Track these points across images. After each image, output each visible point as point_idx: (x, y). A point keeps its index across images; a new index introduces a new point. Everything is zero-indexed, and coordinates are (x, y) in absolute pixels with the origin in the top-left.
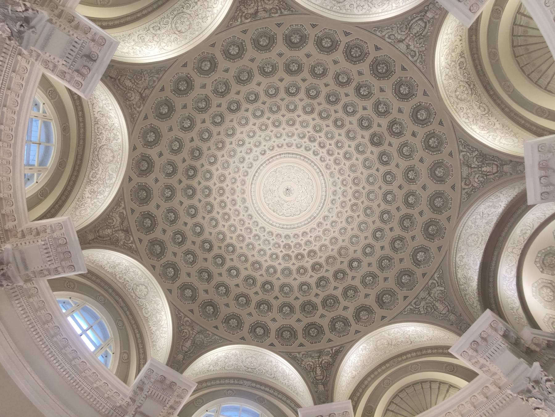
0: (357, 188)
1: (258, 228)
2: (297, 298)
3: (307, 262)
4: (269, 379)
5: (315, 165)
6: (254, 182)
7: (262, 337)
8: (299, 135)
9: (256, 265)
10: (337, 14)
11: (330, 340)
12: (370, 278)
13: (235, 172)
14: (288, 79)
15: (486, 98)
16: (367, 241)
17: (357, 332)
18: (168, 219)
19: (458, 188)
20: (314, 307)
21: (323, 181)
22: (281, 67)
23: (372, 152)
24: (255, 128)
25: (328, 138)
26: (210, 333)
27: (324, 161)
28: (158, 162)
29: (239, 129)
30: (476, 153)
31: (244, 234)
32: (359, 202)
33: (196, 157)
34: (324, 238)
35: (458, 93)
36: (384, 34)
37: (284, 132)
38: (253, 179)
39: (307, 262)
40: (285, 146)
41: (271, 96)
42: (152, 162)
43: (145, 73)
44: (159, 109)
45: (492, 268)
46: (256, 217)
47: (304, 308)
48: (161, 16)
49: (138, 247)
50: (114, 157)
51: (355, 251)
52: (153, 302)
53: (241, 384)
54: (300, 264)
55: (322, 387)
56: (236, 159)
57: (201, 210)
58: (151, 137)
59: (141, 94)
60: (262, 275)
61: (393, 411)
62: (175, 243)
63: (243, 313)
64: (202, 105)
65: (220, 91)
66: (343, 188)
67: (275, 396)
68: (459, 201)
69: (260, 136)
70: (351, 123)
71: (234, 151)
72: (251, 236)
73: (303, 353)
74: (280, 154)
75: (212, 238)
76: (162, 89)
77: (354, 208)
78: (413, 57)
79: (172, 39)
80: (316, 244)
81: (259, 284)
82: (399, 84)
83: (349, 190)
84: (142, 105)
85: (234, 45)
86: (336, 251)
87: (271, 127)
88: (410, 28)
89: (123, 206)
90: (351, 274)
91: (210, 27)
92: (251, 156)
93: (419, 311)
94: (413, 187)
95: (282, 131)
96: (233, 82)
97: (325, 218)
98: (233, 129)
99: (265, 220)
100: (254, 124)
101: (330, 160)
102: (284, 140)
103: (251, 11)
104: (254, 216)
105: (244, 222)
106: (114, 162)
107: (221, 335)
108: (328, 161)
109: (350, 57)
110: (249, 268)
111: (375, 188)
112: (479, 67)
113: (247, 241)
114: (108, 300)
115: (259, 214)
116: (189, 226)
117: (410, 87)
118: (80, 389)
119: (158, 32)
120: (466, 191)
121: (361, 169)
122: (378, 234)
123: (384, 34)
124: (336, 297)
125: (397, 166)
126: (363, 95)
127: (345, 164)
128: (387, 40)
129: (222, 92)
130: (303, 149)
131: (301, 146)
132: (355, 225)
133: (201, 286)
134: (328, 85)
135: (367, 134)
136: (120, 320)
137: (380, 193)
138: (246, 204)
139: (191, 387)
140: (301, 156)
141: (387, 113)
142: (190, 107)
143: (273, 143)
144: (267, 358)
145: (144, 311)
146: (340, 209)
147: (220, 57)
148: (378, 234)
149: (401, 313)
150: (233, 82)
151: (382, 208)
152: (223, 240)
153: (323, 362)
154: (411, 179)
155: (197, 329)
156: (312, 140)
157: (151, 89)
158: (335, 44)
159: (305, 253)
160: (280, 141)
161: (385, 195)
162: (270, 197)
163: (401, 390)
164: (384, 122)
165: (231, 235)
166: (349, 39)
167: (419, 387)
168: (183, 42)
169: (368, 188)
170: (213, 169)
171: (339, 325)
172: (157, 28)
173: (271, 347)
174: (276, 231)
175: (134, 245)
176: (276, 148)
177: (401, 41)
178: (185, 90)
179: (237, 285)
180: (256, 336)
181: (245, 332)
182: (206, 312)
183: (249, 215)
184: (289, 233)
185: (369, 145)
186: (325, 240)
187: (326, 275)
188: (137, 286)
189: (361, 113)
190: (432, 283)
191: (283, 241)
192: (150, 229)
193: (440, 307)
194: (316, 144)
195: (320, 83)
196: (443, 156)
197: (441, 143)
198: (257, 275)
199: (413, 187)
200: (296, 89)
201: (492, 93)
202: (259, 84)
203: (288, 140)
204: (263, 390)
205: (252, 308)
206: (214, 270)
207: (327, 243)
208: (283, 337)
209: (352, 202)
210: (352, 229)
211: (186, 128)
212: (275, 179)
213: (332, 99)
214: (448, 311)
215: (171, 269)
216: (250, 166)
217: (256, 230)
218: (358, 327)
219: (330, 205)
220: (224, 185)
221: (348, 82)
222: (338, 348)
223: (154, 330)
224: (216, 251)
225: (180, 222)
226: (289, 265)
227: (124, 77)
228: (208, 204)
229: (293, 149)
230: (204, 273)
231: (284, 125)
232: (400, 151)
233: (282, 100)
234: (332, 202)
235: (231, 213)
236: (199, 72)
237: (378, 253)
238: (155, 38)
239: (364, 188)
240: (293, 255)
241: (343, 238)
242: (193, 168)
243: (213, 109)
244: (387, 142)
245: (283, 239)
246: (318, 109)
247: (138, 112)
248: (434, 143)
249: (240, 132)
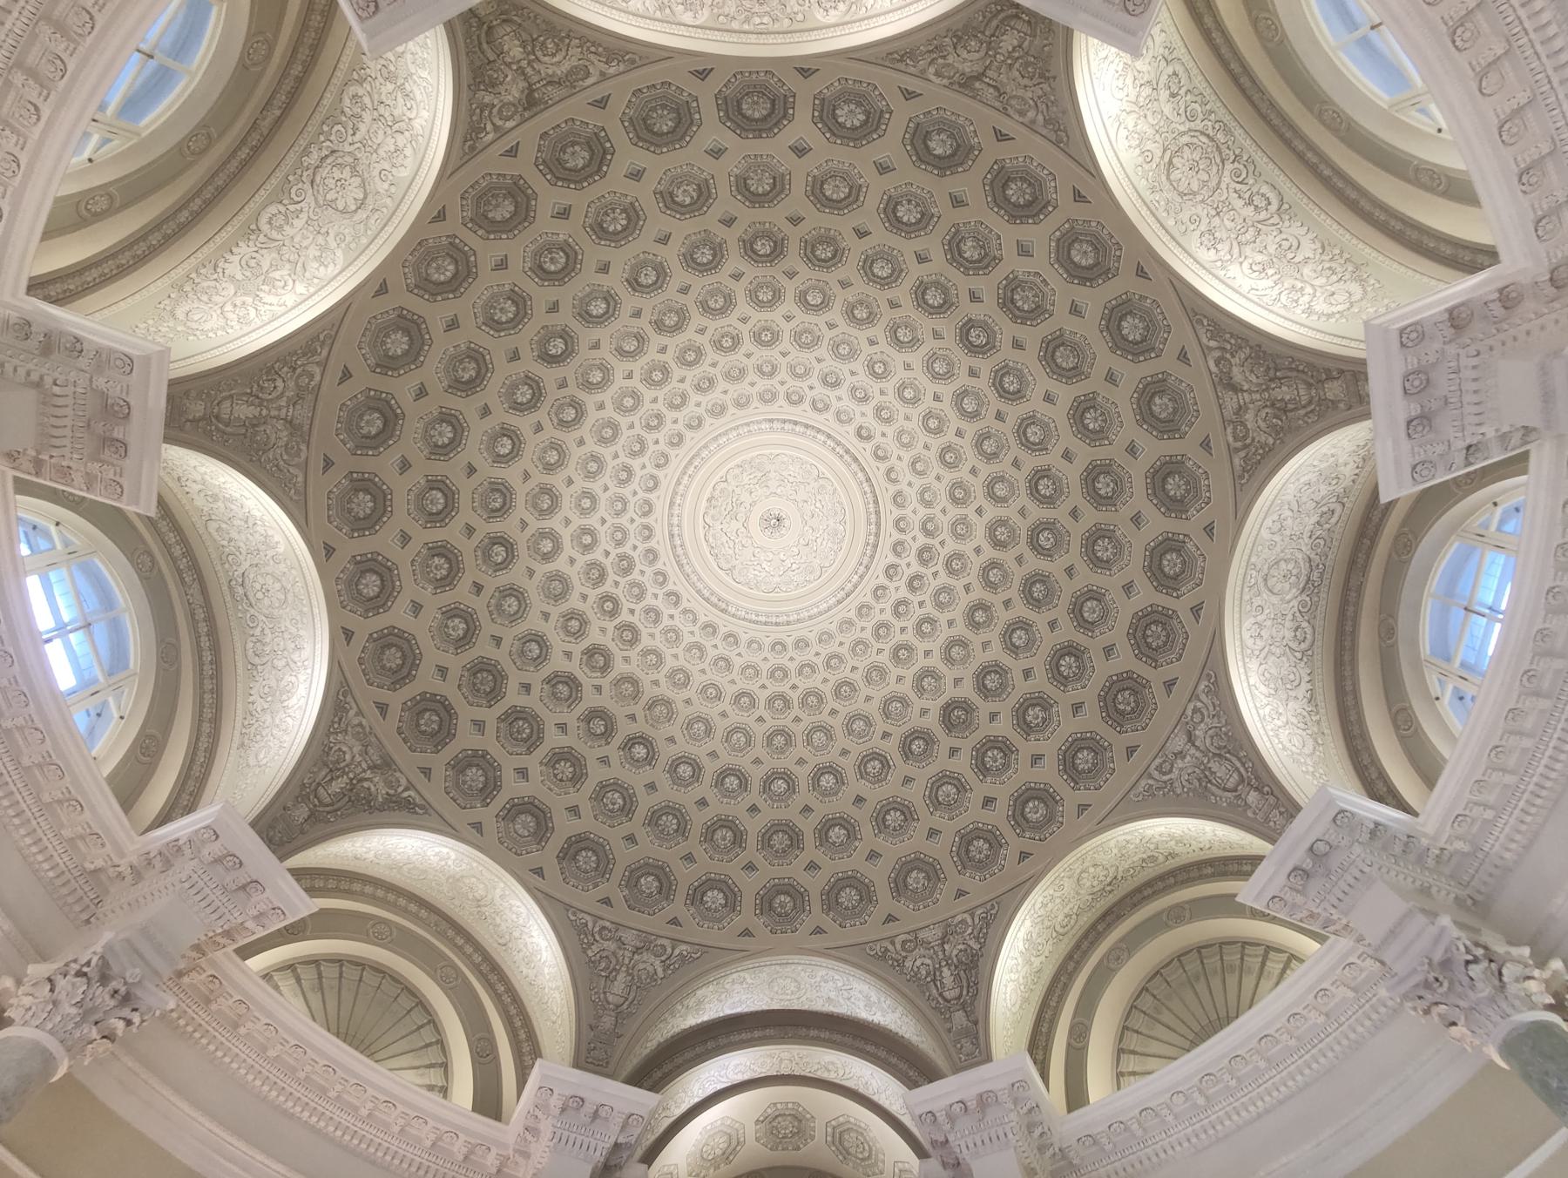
1: (650, 469)
2: (498, 641)
3: (603, 630)
4: (239, 651)
5: (862, 577)
6: (776, 425)
7: (358, 597)
8: (930, 519)
10: (1239, 583)
11: (427, 772)
12: (620, 801)
14: (1072, 474)
15: (1086, 920)
16: (705, 761)
17: (478, 827)
24: (928, 403)
25: (938, 593)
26: (303, 456)
27: (877, 598)
28: (776, 148)
29: (916, 358)
30: (976, 946)
31: (624, 438)
33: (813, 252)
34: (680, 651)
35: (1092, 870)
38: (784, 421)
39: (603, 630)
40: (893, 489)
41: (1021, 432)
42: (770, 129)
45: (736, 1038)
46: (678, 457)
47: (480, 671)
48: (1209, 91)
49: (490, 150)
51: (672, 740)
52: (320, 239)
53: (182, 579)
54: (590, 615)
56: (830, 364)
57: (658, 299)
58: (849, 116)
59: (979, 77)
61: (320, 977)
62: (538, 254)
63: (402, 516)
65: (1017, 297)
66: (819, 661)
67: (201, 684)
69: (909, 419)
70: (985, 645)
71: (853, 354)
72: (623, 459)
73: (364, 722)
74: (868, 480)
75: (584, 354)
76: (1001, 137)
77: (779, 704)
78: (1159, 769)
79: (1150, 145)
80: (658, 635)
81: (497, 527)
85: (1147, 328)
86: (656, 691)
87: (937, 443)
88: (1220, 755)
89: (612, 71)
90: (612, 750)
91: (1189, 261)
92: (848, 404)
94: (867, 830)
96: (1046, 328)
97: (731, 638)
98: (914, 342)
99: (678, 483)
100: (937, 398)
101: (882, 611)
103: (1237, 375)
104: (681, 451)
105: (656, 428)
107: (310, 490)
108: (878, 607)
109: (1143, 622)
110: (532, 483)
111: (842, 741)
112: (1149, 891)
113: (606, 452)
115: (690, 462)
116: (602, 279)
117: (1095, 771)
119: (1164, 94)
120: (890, 947)
121: (879, 693)
124: (540, 739)
125: (908, 780)
126: (1058, 666)
127: (880, 651)
128: (1191, 706)
129: (1013, 301)
130: (897, 536)
131: (902, 531)
132: (736, 717)
133: (432, 370)
134: (1071, 576)
135: (967, 691)
136: (209, 136)
137: (831, 756)
138: (708, 421)
140: (877, 535)
142: (959, 216)
144: (302, 633)
145: (273, 209)
147: (1109, 291)
148: (731, 782)
150: (1046, 328)
152: (589, 386)
153: (366, 784)
154: (884, 820)
155: (300, 413)
156: (925, 555)
157: (997, 104)
158: (1171, 583)
159: (625, 617)
160: (905, 476)
161: (830, 769)
162: (746, 480)
164: (1004, 727)
166: (1185, 616)
167: (406, 1002)
169: (837, 723)
170: (789, 305)
171: (474, 776)
172: (1174, 89)
173: (342, 636)
174: (659, 520)
175: (490, 137)
176: (883, 466)
177: (1191, 738)
178: (1007, 199)
179: (472, 470)
180: (353, 584)
181: (351, 547)
182: (361, 417)
183: (680, 437)
184: (663, 558)
185: (942, 701)
186: (676, 656)
190: (663, 946)
191: (635, 547)
194: (916, 568)
195: (1073, 554)
196: (954, 878)
197: (981, 866)
198: (521, 510)
199: (867, 830)
202: (1046, 398)
203: (912, 494)
205: (423, 536)
207: (670, 663)
208: (383, 653)
209: (790, 692)
211: (894, 211)
212: (800, 479)
214: (618, 1007)
215: (451, 267)
216: (820, 406)
218: (491, 825)
219: (767, 642)
220: (748, 345)
225: (605, 252)
227: (1026, 28)
229: (890, 513)
231: (949, 476)
233: (1016, 464)
235: (673, 384)
237: (686, 798)
238: (1147, 91)
239: (833, 712)
240: (608, 587)
242: (778, 250)
243: (961, 283)
244: (957, 743)
245: (642, 547)
246: (1007, 557)
247: (923, 71)
248: (977, 848)
249: (909, 360)
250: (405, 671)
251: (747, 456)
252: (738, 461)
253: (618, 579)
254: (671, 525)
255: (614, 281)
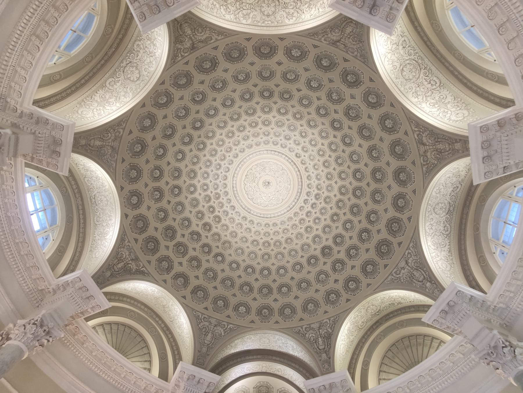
0: (283, 243)
1: (227, 165)
3: (209, 217)
4: (92, 220)
5: (296, 203)
7: (130, 204)
9: (193, 175)
10: (425, 210)
11: (149, 262)
12: (212, 275)
13: (275, 133)
14: (368, 171)
15: (370, 324)
17: (165, 281)
18: (216, 83)
19: (301, 323)
20: (172, 237)
21: (283, 212)
22: (378, 164)
23: (316, 250)
24: (319, 146)
26: (116, 158)
28: (271, 63)
29: (316, 131)
30: (331, 331)
32: (272, 247)
33: (283, 96)
34: (234, 225)
35: (371, 307)
36: (411, 249)
37: (320, 171)
38: (272, 151)
39: (209, 217)
40: (307, 174)
41: (351, 157)
42: (270, 57)
43: (361, 44)
44: (325, 58)
46: (236, 161)
47: (168, 229)
50: (268, 16)
51: (230, 255)
52: (125, 90)
53: (75, 196)
54: (205, 212)
55: (109, 275)
56: (287, 132)
57: (231, 110)
59: (339, 41)
60: (185, 182)
62: (193, 95)
63: (146, 178)
64: (334, 96)
65: (350, 112)
66: (281, 231)
68: (291, 326)
69: (313, 151)
71: (295, 129)
72: (218, 161)
73: (130, 245)
74: (299, 171)
75: (207, 127)
76: (346, 60)
77: (266, 244)
78: (395, 273)
79: (396, 64)
81: (176, 182)
82: (373, 263)
83: (280, 236)
84: (327, 43)
85: (394, 124)
86: (226, 238)
87: (322, 159)
88: (417, 269)
89: (219, 38)
90: (210, 257)
91: (408, 102)
92: (293, 146)
93: (200, 323)
95: (321, 170)
96: (360, 123)
97: (252, 222)
98: (315, 126)
99: (236, 170)
102: (313, 173)
104: (237, 159)
105: (229, 152)
106: (264, 17)
108: (301, 213)
109: (391, 222)
110: (188, 169)
113: (213, 159)
114: (109, 37)
115: (240, 163)
118: (8, 54)
119: (401, 47)
120: (301, 329)
121: (300, 242)
122: (250, 270)
123: (411, 249)
124: (187, 253)
126: (361, 236)
127: (301, 228)
129: (349, 113)
130: (308, 190)
132: (252, 248)
133: (158, 131)
134: (366, 205)
137: (283, 263)
138: (247, 150)
139: (62, 172)
140: (301, 189)
141: (350, 257)
142: (331, 85)
143: (308, 163)
144: (112, 215)
146: (262, 232)
147: (382, 111)
149: (193, 310)
150: (360, 123)
151: (271, 267)
152: (208, 137)
153: (129, 265)
156: (317, 197)
157: (344, 50)
159: (217, 213)
160: (311, 170)
161: (283, 267)
162: (258, 170)
163: (130, 328)
164: (342, 256)
165: (214, 143)
166: (405, 220)
168: (393, 76)
169: (286, 252)
170: (274, 113)
171: (165, 264)
172: (404, 45)
174: (229, 182)
175: (180, 58)
176: (304, 166)
177: (407, 263)
178: (347, 80)
179: (169, 163)
180: (129, 199)
182: (134, 146)
183: (237, 155)
187: (203, 237)
188: (136, 67)
189: (347, 235)
190: (224, 325)
192: (201, 69)
193: (209, 337)
194: (314, 201)
195: (367, 198)
196: (324, 307)
197: (333, 303)
198: (184, 177)
200: (360, 179)
201: (374, 327)
202: (360, 145)
203: (313, 176)
204: (79, 218)
205: (153, 184)
206: (176, 139)
207: (231, 229)
210: (248, 247)
211: (310, 83)
212: (276, 170)
213: (355, 210)
214: (208, 345)
215: (165, 99)
217: (225, 164)
218: (169, 281)
219: (264, 223)
220: (260, 125)
221: (371, 222)
222: (146, 271)
223: (96, 98)
224: (195, 134)
225: (215, 94)
226: (202, 203)
227: (354, 26)
228: (239, 115)
229: (306, 182)
230: (171, 130)
231: (326, 171)
232: (321, 272)
233: (349, 167)
234: (266, 224)
235: (236, 137)
236: (366, 92)
237: (234, 275)
238: (395, 46)
239: (285, 248)
240: (211, 203)
241: (238, 242)
242: (271, 95)
243: (332, 107)
245: (223, 190)
246: (345, 198)
247: (320, 39)
249: (314, 132)
250: (144, 229)
251: (259, 162)
252: (256, 163)
253: (215, 201)
254: (233, 184)
255: (218, 104)
